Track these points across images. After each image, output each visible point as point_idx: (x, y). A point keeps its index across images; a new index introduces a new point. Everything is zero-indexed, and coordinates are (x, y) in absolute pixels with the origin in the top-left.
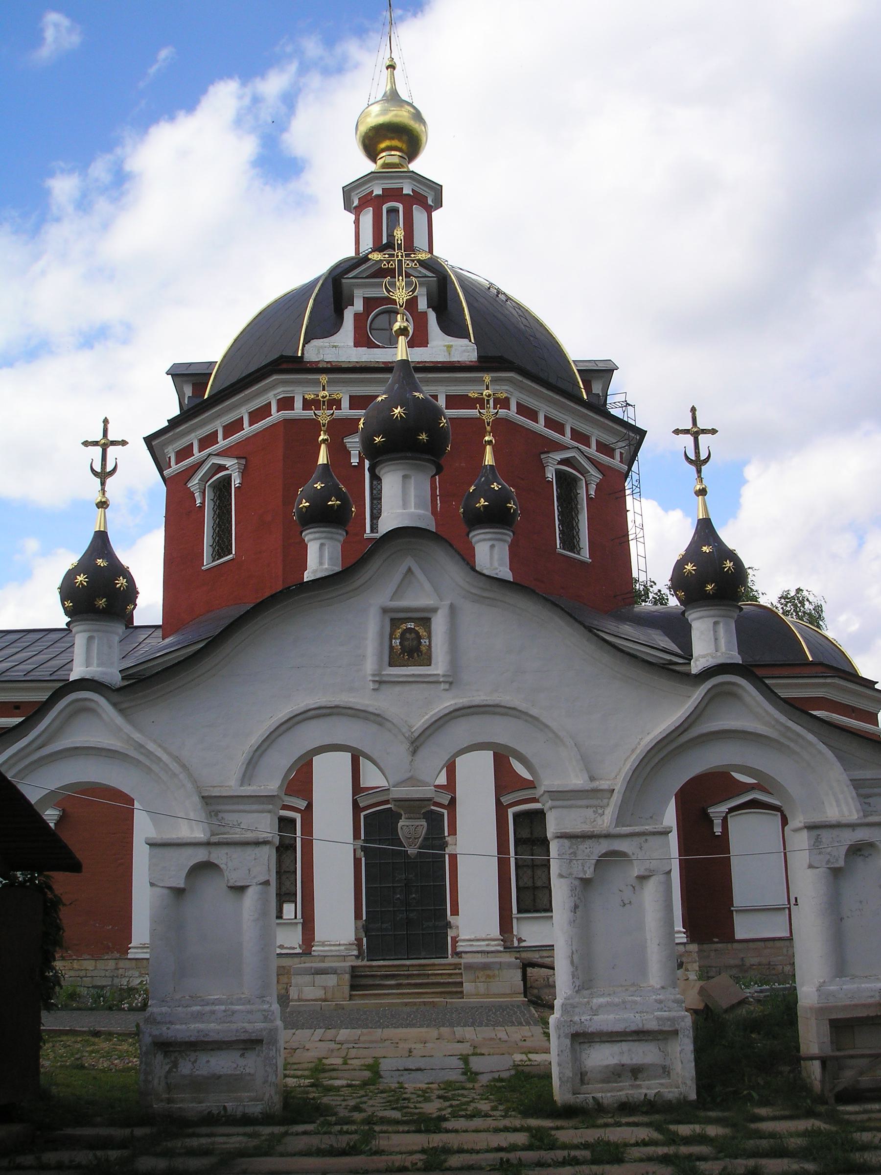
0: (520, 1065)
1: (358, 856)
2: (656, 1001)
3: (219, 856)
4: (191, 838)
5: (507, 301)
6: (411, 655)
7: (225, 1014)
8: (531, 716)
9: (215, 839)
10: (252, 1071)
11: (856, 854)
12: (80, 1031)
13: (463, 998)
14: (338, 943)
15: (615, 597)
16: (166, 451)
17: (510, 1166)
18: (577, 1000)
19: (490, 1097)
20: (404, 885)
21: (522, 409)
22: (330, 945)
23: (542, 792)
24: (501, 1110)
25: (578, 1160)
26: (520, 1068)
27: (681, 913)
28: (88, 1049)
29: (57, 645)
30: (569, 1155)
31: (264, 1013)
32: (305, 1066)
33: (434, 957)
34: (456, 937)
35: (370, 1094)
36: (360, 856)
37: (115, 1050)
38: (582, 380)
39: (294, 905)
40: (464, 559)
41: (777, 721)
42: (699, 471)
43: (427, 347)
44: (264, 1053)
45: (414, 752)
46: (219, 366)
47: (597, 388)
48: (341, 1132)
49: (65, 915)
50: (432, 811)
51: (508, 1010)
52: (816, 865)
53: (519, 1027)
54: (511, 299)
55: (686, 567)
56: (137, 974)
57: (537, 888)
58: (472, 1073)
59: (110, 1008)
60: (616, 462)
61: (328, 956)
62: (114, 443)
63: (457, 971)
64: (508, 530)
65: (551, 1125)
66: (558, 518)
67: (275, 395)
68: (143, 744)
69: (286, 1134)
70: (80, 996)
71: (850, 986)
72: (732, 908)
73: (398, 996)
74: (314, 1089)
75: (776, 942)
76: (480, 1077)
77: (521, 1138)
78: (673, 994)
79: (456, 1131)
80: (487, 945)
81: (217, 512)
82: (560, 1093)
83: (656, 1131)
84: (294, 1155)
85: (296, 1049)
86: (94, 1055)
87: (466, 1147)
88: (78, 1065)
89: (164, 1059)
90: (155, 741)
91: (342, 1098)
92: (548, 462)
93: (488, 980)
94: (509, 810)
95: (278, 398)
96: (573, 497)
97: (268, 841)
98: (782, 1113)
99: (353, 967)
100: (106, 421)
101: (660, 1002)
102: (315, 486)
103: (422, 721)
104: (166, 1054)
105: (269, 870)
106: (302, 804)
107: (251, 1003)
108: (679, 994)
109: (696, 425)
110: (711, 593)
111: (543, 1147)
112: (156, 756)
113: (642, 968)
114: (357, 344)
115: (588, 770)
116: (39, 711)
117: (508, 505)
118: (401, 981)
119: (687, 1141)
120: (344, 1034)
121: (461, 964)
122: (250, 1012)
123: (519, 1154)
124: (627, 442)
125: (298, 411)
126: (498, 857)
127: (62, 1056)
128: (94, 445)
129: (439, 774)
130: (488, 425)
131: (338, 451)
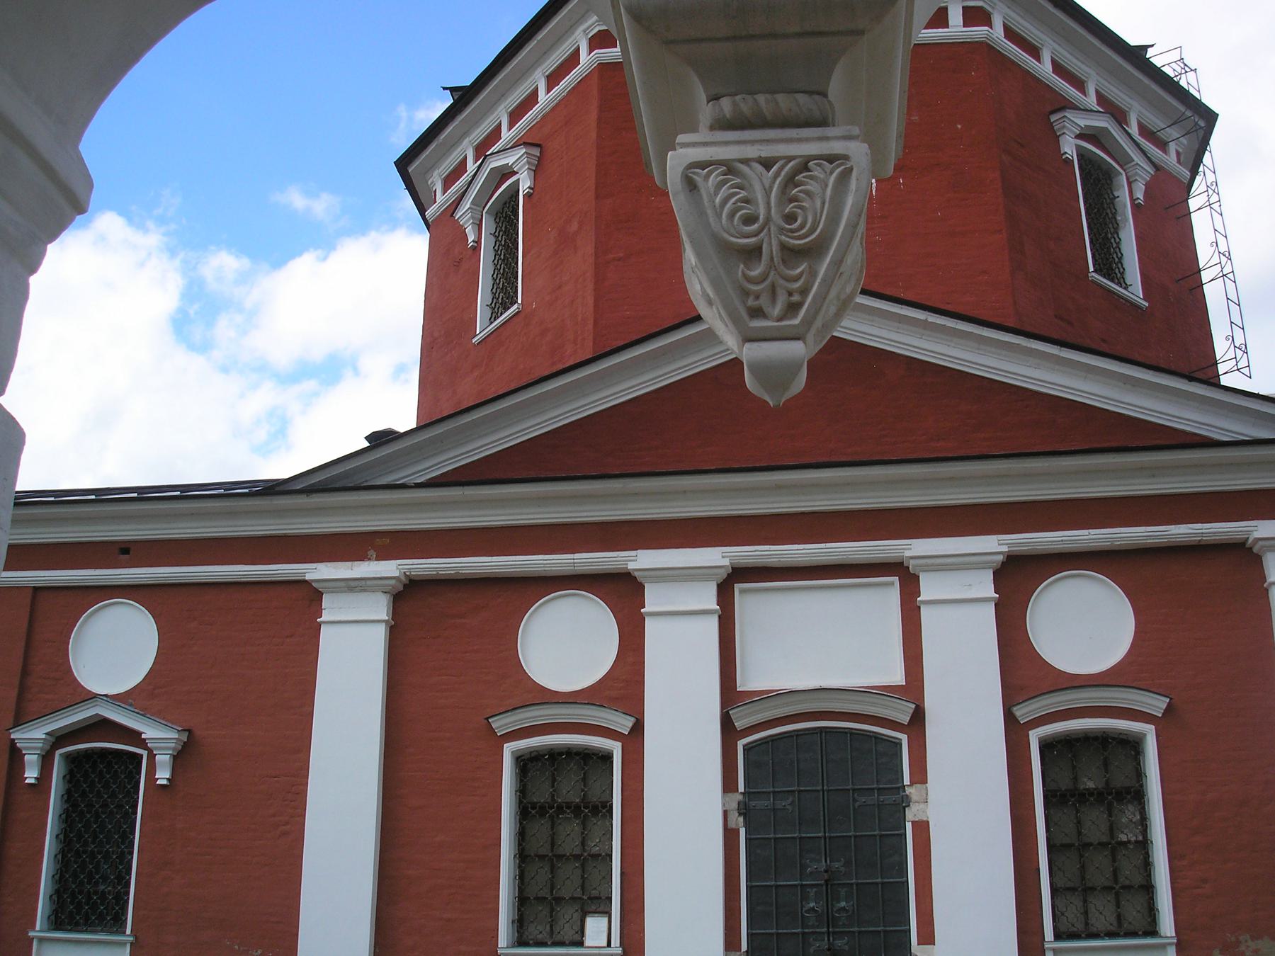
1: (732, 825)
20: (823, 882)
36: (737, 824)
39: (606, 920)
67: (584, 31)
92: (1064, 127)
94: (1031, 732)
106: (624, 724)
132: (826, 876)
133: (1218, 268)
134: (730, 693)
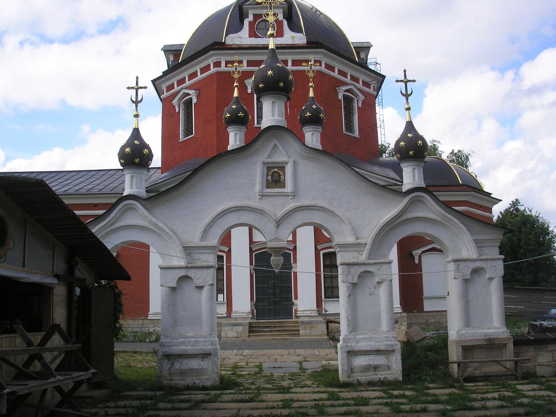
0: (325, 366)
1: (252, 273)
2: (385, 337)
3: (191, 273)
4: (179, 265)
5: (320, 14)
6: (276, 184)
7: (194, 342)
8: (330, 211)
9: (189, 265)
10: (206, 367)
11: (476, 273)
12: (128, 351)
13: (300, 337)
14: (243, 312)
15: (370, 153)
16: (161, 87)
17: (319, 407)
18: (350, 336)
19: (311, 379)
21: (328, 66)
22: (240, 313)
23: (335, 245)
24: (316, 385)
25: (349, 404)
26: (325, 367)
27: (399, 299)
28: (132, 359)
29: (113, 177)
30: (345, 402)
31: (211, 342)
32: (229, 366)
33: (287, 318)
34: (296, 310)
35: (258, 378)
37: (144, 359)
38: (355, 52)
39: (223, 295)
40: (300, 140)
41: (440, 213)
42: (407, 99)
43: (283, 37)
44: (212, 359)
45: (278, 227)
46: (186, 46)
47: (362, 56)
48: (246, 393)
49: (124, 300)
50: (286, 252)
51: (320, 342)
52: (458, 278)
53: (325, 349)
54: (322, 14)
55: (401, 143)
56: (152, 326)
57: (334, 287)
58: (303, 369)
59: (141, 341)
60: (371, 91)
61: (238, 318)
62: (141, 88)
63: (297, 325)
64: (320, 126)
65: (338, 390)
66: (344, 117)
67: (212, 60)
68: (157, 223)
69: (222, 394)
70: (126, 336)
71: (471, 331)
72: (423, 297)
73: (270, 336)
74: (233, 376)
75: (443, 312)
76: (307, 371)
77: (325, 396)
78: (392, 334)
79: (296, 393)
80: (311, 313)
81: (186, 115)
82: (342, 377)
83: (383, 393)
84: (226, 402)
85: (225, 359)
86: (135, 361)
87: (300, 399)
88: (128, 366)
89: (168, 362)
90: (162, 222)
91: (246, 379)
92: (339, 91)
93: (311, 329)
94: (321, 252)
95: (213, 62)
96: (351, 107)
97: (213, 266)
98: (440, 386)
99: (250, 323)
100: (137, 78)
101: (387, 337)
102: (233, 107)
103: (281, 213)
104: (169, 360)
105: (213, 279)
106: (226, 249)
107: (206, 337)
108: (395, 334)
109: (406, 78)
110: (412, 155)
111: (334, 399)
112: (163, 229)
113: (379, 323)
114: (250, 36)
115: (355, 234)
116: (111, 208)
117: (320, 115)
118: (271, 329)
119: (397, 397)
120: (246, 352)
121: (299, 322)
122: (206, 341)
123: (323, 402)
124: (377, 81)
125: (223, 68)
126: (316, 274)
127: (121, 362)
128: (132, 89)
129: (289, 236)
130: (311, 78)
131: (243, 88)
132: (273, 284)
133: (380, 125)
134: (251, 242)
